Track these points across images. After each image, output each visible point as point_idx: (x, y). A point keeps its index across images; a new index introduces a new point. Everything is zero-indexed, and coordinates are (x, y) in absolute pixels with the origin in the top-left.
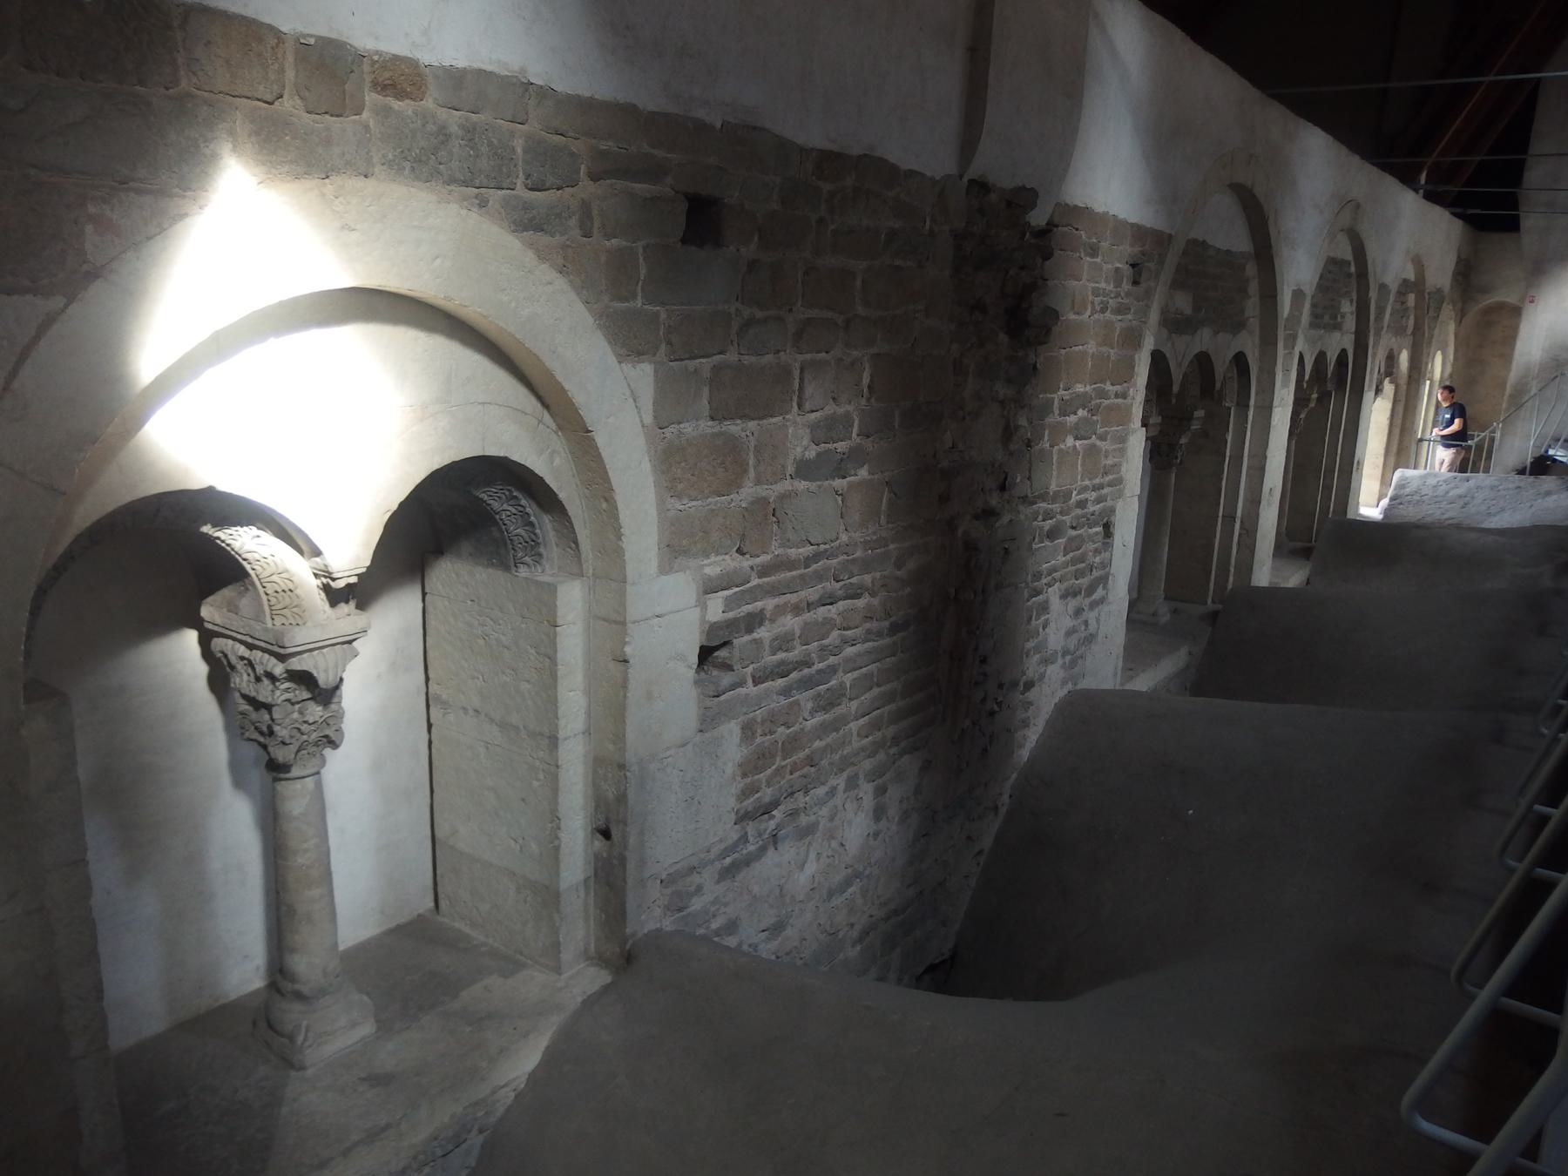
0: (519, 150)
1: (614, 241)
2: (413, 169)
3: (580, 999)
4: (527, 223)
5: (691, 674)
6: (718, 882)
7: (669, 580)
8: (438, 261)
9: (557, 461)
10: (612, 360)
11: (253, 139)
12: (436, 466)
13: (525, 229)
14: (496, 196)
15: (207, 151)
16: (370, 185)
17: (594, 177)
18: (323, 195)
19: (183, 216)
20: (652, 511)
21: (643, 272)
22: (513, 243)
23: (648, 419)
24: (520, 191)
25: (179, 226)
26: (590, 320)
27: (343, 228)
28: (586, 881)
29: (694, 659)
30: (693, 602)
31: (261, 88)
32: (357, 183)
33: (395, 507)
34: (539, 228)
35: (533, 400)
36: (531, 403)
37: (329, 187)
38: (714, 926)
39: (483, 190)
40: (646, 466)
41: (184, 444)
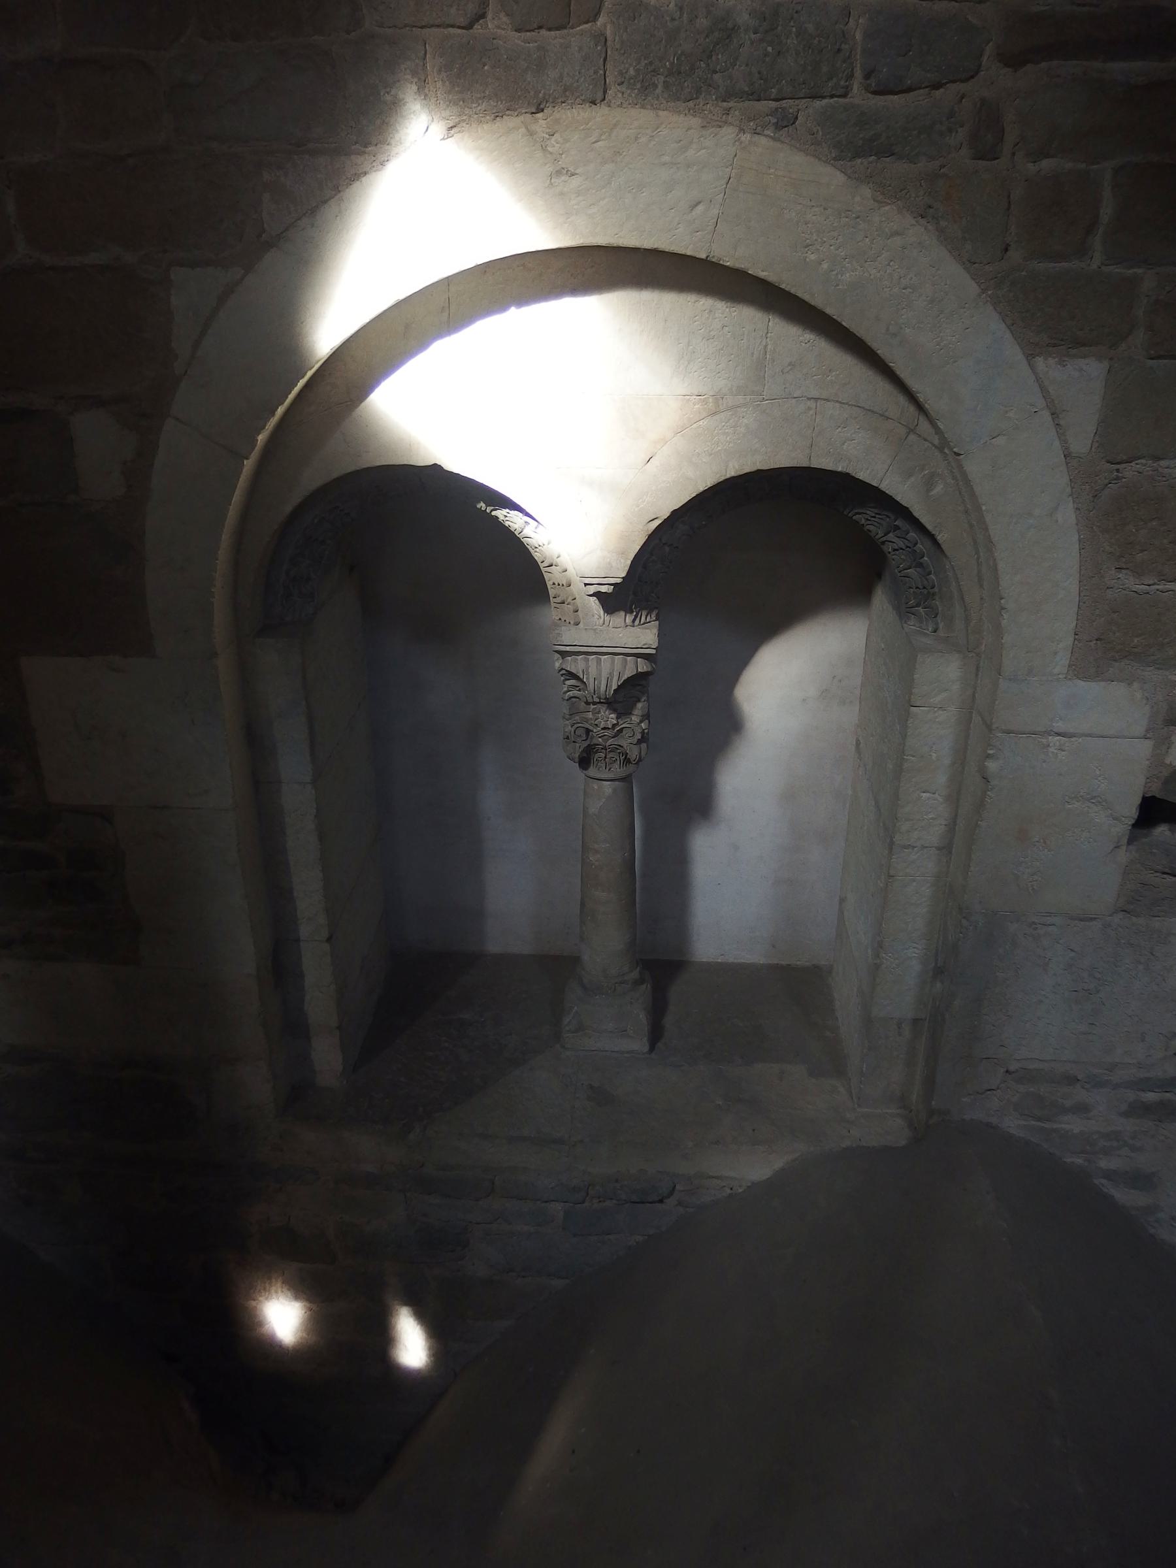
0: (859, 36)
1: (1046, 164)
2: (666, 85)
3: (847, 1143)
4: (860, 146)
5: (1122, 829)
6: (1125, 1114)
7: (1090, 689)
8: (700, 208)
9: (939, 489)
10: (1013, 352)
11: (444, 74)
12: (731, 473)
13: (857, 155)
14: (809, 111)
15: (388, 98)
16: (600, 114)
17: (1013, 60)
18: (531, 133)
19: (358, 176)
20: (1068, 585)
21: (1107, 212)
22: (832, 178)
23: (1082, 442)
24: (858, 96)
25: (356, 185)
26: (973, 288)
27: (559, 173)
28: (915, 1021)
29: (1130, 810)
30: (1140, 729)
31: (453, 11)
32: (581, 113)
33: (665, 514)
34: (887, 151)
35: (902, 399)
36: (896, 403)
37: (541, 123)
38: (1103, 1164)
39: (784, 103)
40: (1067, 515)
41: (424, 414)
